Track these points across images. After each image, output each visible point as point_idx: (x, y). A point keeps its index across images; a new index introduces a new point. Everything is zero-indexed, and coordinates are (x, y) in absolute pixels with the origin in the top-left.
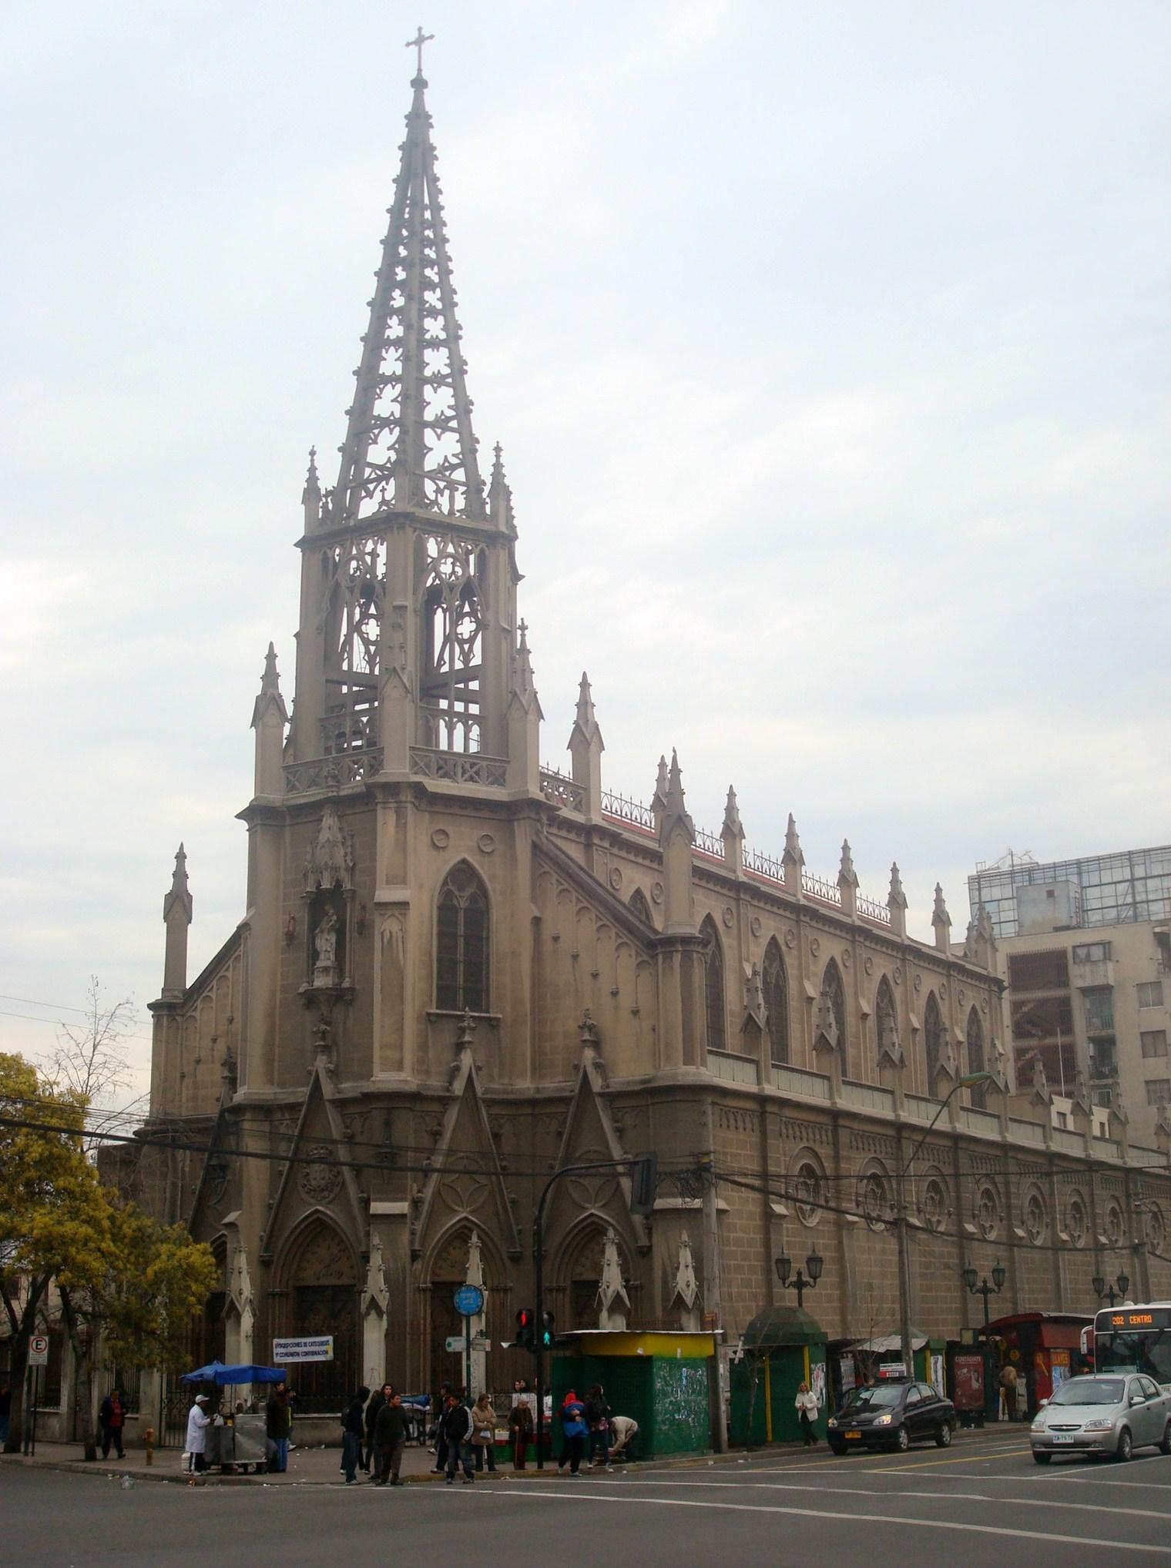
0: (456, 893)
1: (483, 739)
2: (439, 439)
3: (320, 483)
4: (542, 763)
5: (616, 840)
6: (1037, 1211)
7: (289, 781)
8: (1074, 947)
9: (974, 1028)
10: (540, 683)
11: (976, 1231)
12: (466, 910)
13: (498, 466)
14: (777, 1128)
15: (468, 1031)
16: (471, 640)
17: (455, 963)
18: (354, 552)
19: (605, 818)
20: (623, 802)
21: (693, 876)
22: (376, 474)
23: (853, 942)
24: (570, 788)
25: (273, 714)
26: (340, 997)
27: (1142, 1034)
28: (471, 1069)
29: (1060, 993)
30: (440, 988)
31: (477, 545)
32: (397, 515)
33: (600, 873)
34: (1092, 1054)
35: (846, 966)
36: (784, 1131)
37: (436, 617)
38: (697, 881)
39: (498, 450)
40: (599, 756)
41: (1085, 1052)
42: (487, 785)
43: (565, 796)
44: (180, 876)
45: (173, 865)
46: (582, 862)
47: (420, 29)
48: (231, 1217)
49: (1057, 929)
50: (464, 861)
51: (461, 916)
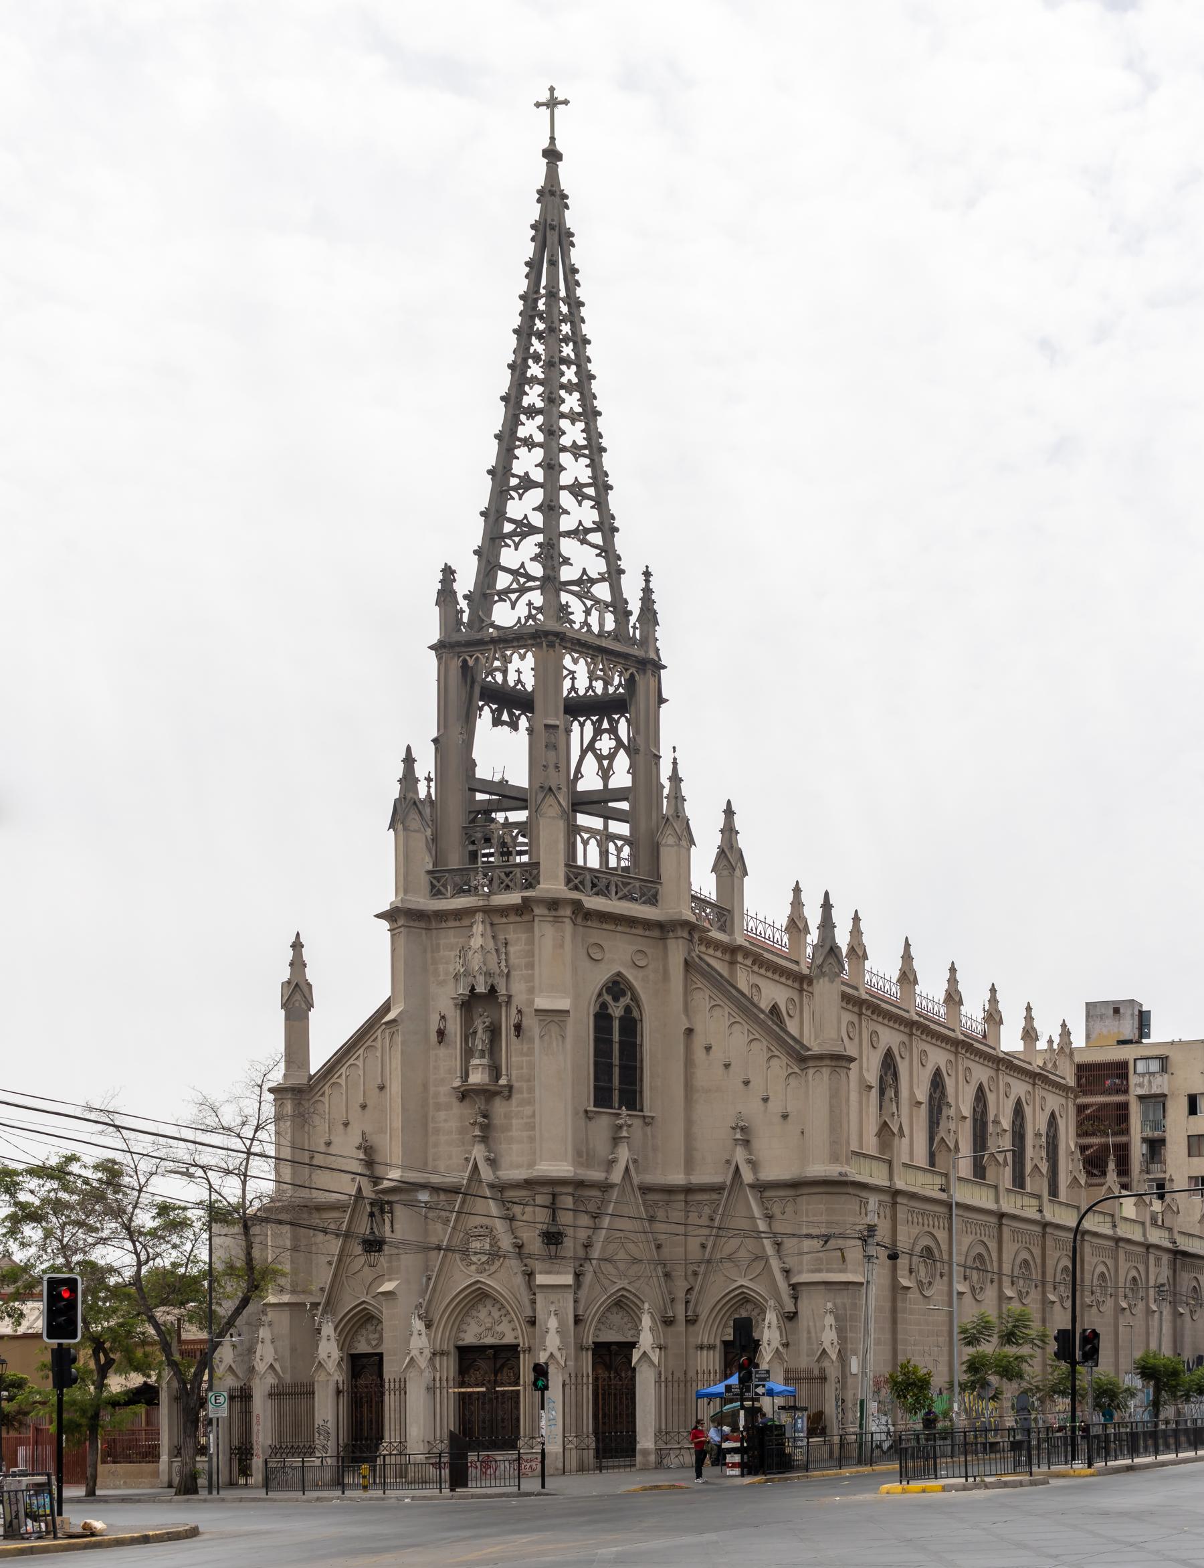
1: (633, 855)
2: (526, 515)
3: (456, 586)
4: (695, 887)
5: (925, 1030)
7: (433, 886)
8: (1135, 1060)
9: (1052, 1130)
10: (690, 810)
11: (1056, 1300)
13: (647, 591)
14: (905, 1216)
15: (625, 1128)
16: (612, 757)
17: (610, 1066)
19: (748, 939)
20: (767, 926)
21: (842, 1001)
23: (1034, 1085)
24: (716, 910)
25: (414, 819)
26: (488, 1094)
28: (628, 1161)
29: (1120, 1098)
30: (596, 1088)
31: (626, 670)
32: (546, 634)
35: (990, 1090)
36: (910, 1218)
38: (844, 1005)
39: (647, 574)
40: (743, 880)
41: (1138, 1150)
42: (640, 904)
43: (697, 911)
44: (298, 964)
45: (289, 954)
46: (725, 974)
47: (552, 89)
48: (388, 1286)
49: (1122, 1042)
50: (619, 974)
51: (616, 1025)
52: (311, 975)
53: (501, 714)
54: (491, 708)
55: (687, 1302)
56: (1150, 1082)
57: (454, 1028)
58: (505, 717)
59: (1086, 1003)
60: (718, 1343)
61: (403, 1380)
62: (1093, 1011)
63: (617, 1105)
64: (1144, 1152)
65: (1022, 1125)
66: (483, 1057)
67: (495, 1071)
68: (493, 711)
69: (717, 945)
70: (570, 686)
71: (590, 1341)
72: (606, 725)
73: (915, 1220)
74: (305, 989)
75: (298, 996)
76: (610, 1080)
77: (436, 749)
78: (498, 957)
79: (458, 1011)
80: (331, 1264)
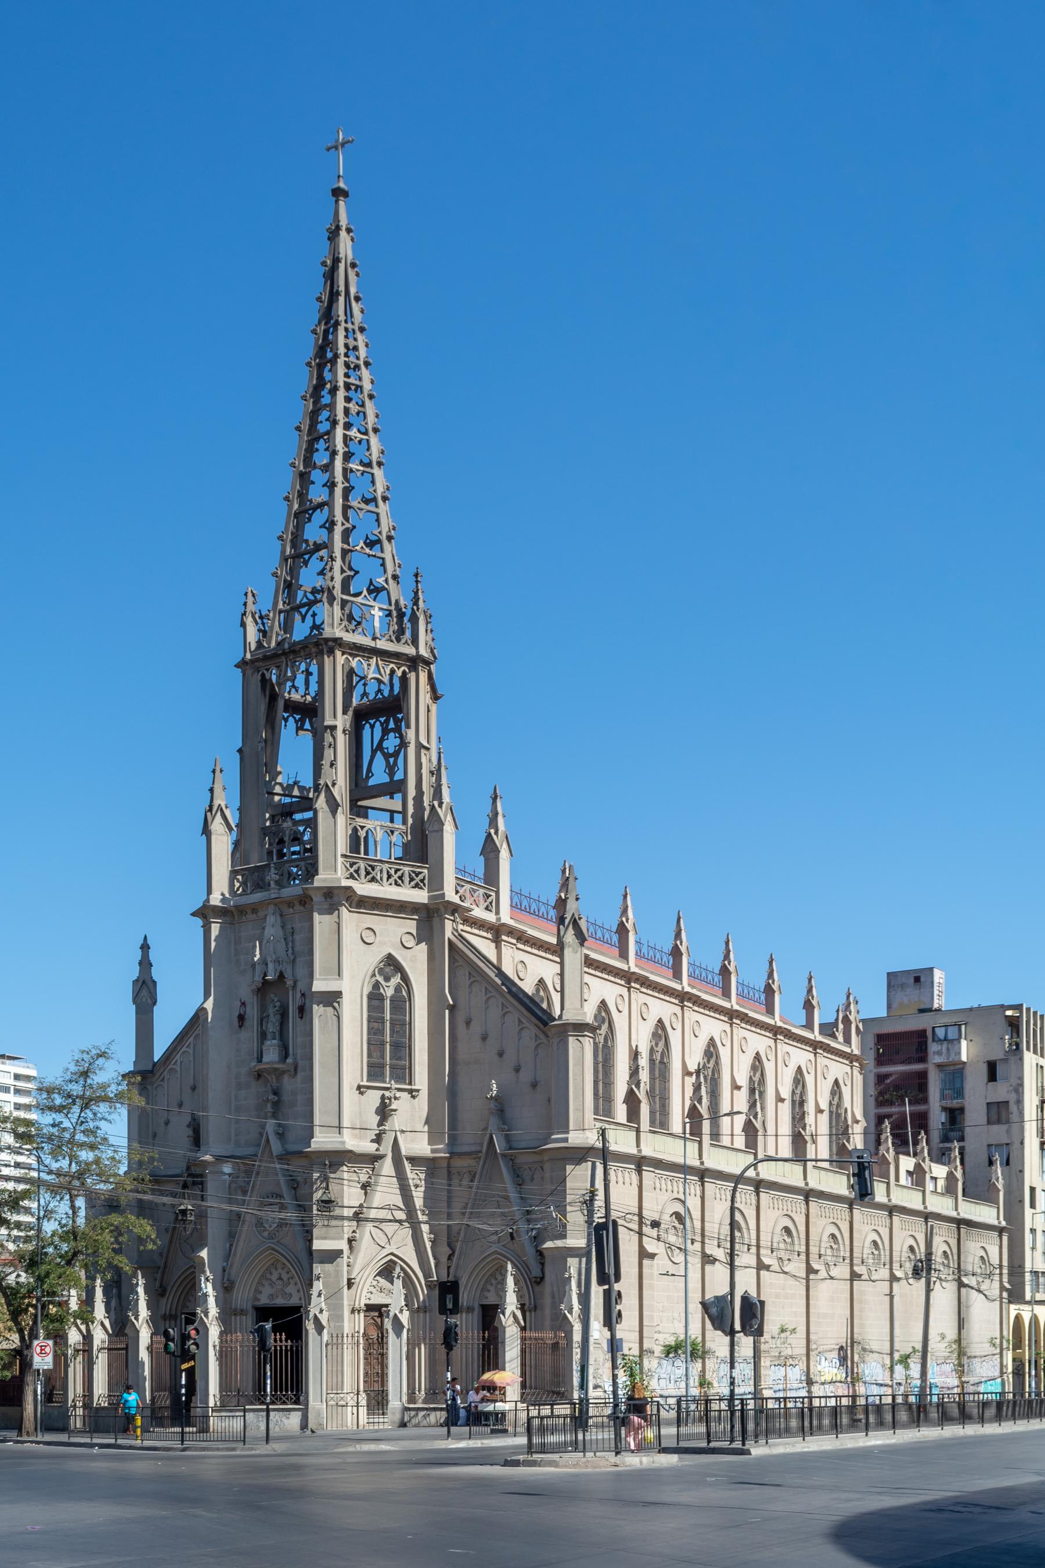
0: (383, 983)
6: (835, 1246)
9: (836, 1099)
12: (392, 997)
18: (289, 674)
22: (307, 598)
27: (988, 1104)
30: (369, 1066)
33: (508, 969)
34: (943, 1121)
37: (364, 732)
44: (145, 964)
51: (387, 1003)
52: (155, 973)
53: (303, 724)
54: (294, 718)
55: (449, 1267)
56: (948, 1050)
57: (252, 1013)
58: (307, 726)
59: (889, 974)
60: (476, 1306)
61: (340, 1336)
62: (895, 981)
63: (388, 1080)
64: (943, 1120)
65: (803, 1093)
66: (274, 1039)
67: (285, 1052)
68: (296, 722)
69: (480, 924)
70: (362, 692)
71: (362, 1305)
72: (392, 725)
73: (664, 1186)
74: (151, 984)
75: (144, 992)
76: (383, 1057)
77: (242, 759)
78: (287, 944)
79: (255, 997)
80: (167, 1232)
